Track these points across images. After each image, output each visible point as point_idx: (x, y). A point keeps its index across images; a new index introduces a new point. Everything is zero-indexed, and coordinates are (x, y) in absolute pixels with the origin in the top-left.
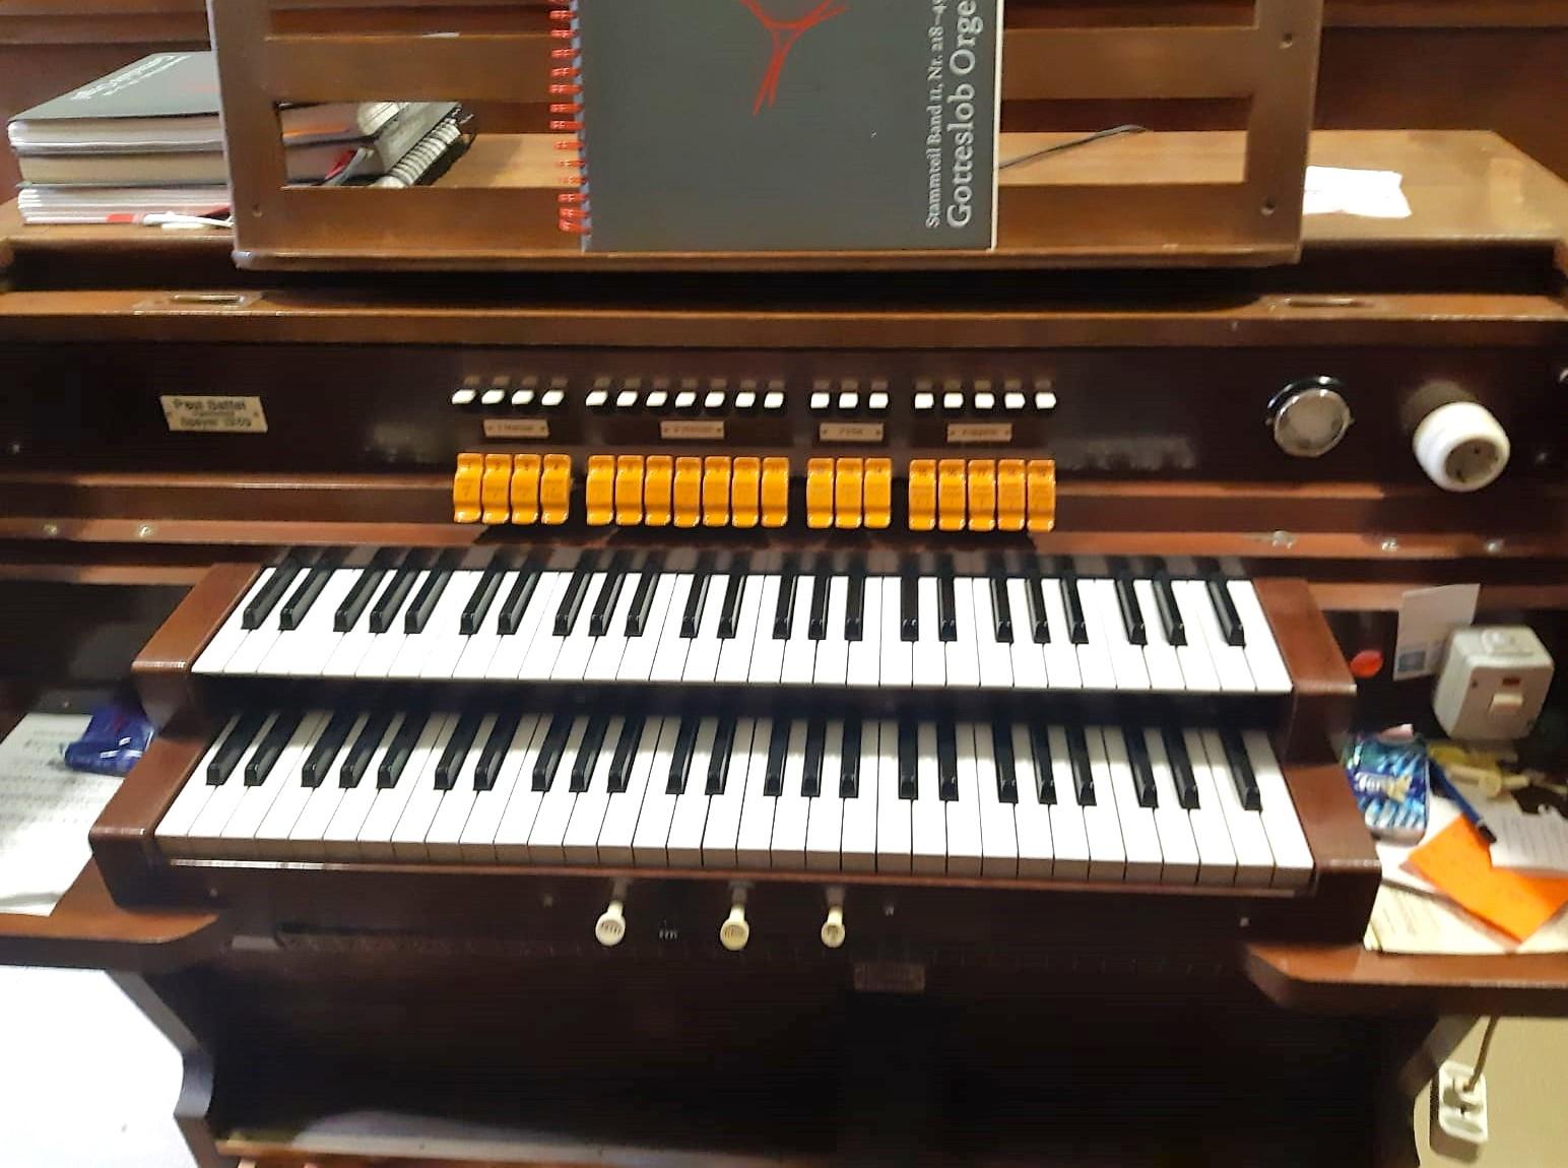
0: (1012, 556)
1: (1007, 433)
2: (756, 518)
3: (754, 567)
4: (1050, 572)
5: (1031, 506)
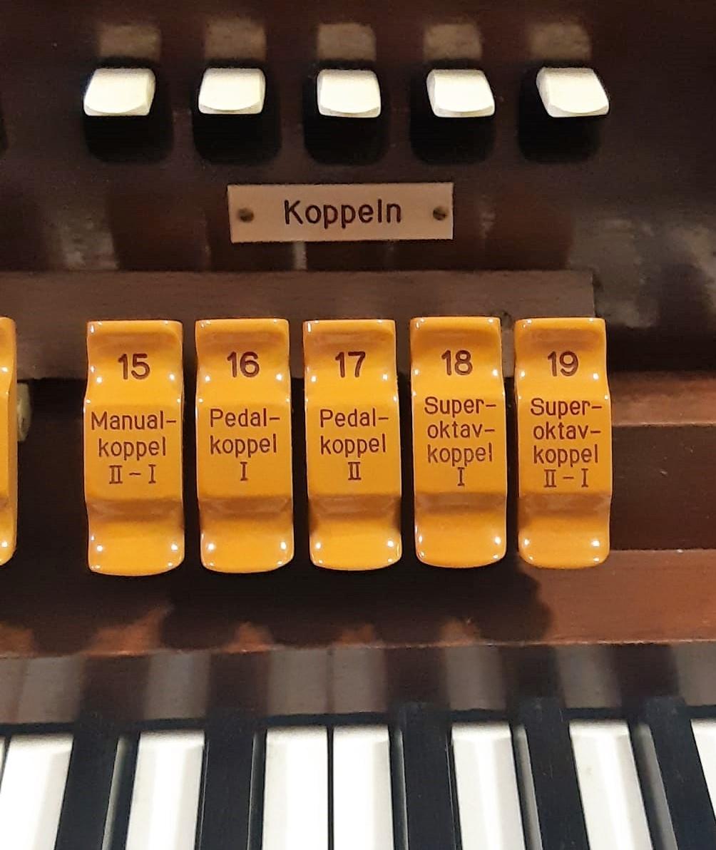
0: (464, 653)
1: (439, 214)
2: (499, 541)
3: (289, 699)
4: (479, 703)
5: (207, 484)
